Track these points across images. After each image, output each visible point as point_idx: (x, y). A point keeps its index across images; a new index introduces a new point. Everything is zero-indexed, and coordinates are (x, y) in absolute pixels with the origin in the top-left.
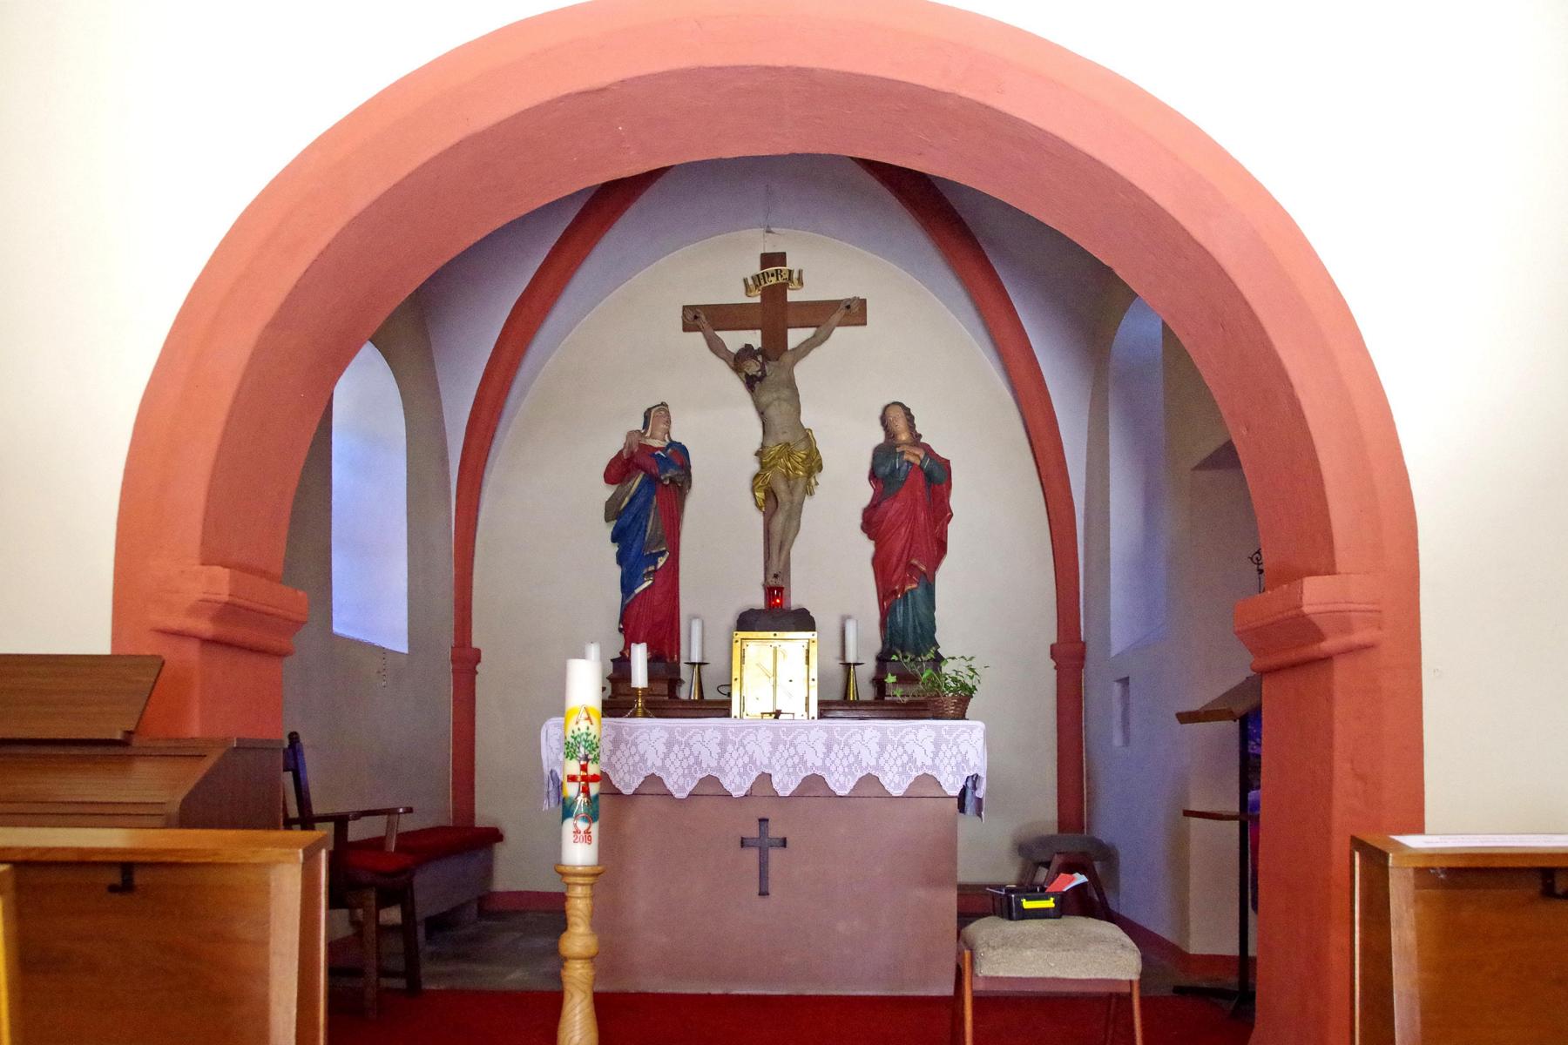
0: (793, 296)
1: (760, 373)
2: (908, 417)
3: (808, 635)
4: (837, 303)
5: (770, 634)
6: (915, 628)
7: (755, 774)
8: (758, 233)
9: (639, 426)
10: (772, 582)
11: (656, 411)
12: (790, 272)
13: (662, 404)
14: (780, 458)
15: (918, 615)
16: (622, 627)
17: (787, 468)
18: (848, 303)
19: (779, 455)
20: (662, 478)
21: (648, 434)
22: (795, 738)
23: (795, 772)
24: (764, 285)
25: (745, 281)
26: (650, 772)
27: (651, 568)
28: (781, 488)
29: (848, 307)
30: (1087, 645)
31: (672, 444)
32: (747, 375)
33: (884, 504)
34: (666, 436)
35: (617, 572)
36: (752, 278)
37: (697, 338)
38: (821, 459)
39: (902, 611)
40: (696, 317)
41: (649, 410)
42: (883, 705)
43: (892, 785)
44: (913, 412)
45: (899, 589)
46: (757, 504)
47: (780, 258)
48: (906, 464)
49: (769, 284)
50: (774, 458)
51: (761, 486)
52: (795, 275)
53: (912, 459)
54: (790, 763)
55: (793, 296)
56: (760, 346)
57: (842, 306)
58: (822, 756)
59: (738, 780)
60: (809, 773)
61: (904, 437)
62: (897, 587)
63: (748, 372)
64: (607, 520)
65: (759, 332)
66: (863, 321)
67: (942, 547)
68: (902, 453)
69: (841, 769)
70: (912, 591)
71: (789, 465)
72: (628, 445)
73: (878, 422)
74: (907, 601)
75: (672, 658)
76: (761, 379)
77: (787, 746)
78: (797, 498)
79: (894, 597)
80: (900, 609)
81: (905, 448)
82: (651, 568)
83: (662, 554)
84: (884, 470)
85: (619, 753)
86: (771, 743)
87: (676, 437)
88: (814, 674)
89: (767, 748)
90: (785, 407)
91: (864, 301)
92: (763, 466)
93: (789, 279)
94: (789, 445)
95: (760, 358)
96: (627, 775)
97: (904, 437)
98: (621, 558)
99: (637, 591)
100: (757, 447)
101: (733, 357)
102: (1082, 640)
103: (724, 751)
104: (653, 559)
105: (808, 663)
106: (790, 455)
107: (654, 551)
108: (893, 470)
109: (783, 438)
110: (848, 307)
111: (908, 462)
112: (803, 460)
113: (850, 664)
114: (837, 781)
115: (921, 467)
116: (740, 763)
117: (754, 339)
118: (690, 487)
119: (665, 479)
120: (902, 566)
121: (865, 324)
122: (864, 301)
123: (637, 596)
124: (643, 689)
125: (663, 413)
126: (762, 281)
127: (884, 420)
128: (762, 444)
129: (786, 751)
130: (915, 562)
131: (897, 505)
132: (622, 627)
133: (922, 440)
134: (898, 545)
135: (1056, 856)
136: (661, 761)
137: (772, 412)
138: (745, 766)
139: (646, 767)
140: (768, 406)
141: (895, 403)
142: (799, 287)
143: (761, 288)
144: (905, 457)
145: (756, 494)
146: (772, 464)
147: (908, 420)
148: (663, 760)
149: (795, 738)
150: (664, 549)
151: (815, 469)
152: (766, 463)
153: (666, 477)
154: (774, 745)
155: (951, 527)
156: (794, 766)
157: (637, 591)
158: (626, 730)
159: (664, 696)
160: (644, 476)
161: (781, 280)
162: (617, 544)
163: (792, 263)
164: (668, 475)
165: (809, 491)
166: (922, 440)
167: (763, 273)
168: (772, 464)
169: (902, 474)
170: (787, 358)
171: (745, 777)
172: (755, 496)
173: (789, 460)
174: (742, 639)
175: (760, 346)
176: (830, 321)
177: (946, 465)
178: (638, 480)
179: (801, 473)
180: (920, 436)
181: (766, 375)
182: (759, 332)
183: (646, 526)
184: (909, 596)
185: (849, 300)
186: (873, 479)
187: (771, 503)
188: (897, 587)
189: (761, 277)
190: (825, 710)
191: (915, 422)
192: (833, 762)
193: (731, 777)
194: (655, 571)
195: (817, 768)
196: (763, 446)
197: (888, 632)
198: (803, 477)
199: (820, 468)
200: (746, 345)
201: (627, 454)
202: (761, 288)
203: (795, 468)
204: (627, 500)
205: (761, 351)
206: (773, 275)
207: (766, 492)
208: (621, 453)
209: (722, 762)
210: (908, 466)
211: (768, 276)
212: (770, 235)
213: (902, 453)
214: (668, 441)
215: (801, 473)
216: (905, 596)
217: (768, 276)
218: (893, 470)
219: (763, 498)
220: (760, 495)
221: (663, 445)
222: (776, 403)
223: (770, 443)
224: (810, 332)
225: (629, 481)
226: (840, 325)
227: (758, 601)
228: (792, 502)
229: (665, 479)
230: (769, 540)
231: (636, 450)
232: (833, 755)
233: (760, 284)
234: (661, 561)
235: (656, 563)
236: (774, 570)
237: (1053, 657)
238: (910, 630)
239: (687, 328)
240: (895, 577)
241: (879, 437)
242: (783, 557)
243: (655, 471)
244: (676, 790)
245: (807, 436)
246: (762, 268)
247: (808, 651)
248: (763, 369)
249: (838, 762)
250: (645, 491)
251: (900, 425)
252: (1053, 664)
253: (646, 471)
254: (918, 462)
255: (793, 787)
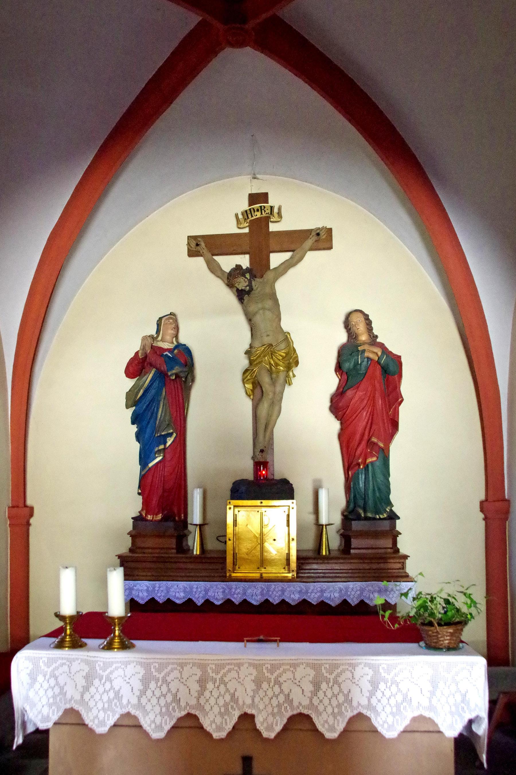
0: (273, 227)
1: (248, 288)
2: (367, 321)
3: (288, 502)
4: (310, 231)
5: (257, 502)
6: (374, 490)
7: (236, 714)
8: (245, 179)
9: (153, 332)
10: (260, 458)
11: (166, 319)
12: (272, 208)
13: (171, 314)
14: (265, 356)
15: (376, 481)
16: (140, 491)
17: (270, 363)
18: (318, 231)
19: (264, 354)
20: (169, 374)
21: (160, 338)
22: (280, 675)
23: (280, 712)
24: (251, 218)
25: (237, 215)
26: (125, 711)
27: (162, 447)
28: (266, 380)
29: (318, 234)
30: (512, 501)
31: (179, 346)
32: (238, 290)
33: (349, 393)
34: (174, 339)
35: (136, 446)
36: (242, 214)
37: (200, 261)
38: (297, 357)
39: (363, 477)
40: (197, 245)
41: (160, 319)
42: (349, 559)
43: (386, 726)
44: (370, 318)
45: (362, 462)
46: (246, 393)
47: (263, 197)
48: (366, 360)
49: (255, 217)
50: (259, 356)
51: (249, 379)
52: (276, 210)
53: (371, 356)
54: (275, 702)
55: (273, 227)
56: (248, 266)
57: (314, 233)
58: (310, 695)
59: (218, 720)
60: (295, 712)
61: (364, 338)
62: (360, 461)
63: (238, 287)
64: (127, 407)
65: (247, 257)
66: (330, 246)
67: (395, 425)
68: (364, 351)
69: (329, 710)
70: (372, 463)
71: (272, 362)
72: (143, 347)
73: (342, 326)
74: (368, 470)
75: (180, 517)
76: (249, 293)
77: (272, 684)
78: (278, 389)
79: (358, 467)
80: (362, 477)
81: (366, 347)
82: (162, 447)
83: (170, 435)
84: (347, 366)
85: (92, 690)
86: (253, 681)
87: (183, 340)
88: (294, 534)
89: (250, 686)
90: (268, 314)
91: (330, 230)
92: (251, 363)
93: (271, 213)
94: (272, 345)
95: (248, 276)
96: (101, 712)
97: (364, 338)
98: (139, 436)
99: (150, 465)
100: (247, 347)
101: (226, 275)
102: (506, 497)
103: (203, 688)
104: (163, 439)
105: (288, 525)
106: (272, 354)
107: (163, 433)
108: (356, 364)
109: (267, 340)
110: (318, 234)
111: (368, 358)
112: (284, 358)
113: (322, 525)
114: (326, 722)
115: (378, 362)
116: (221, 702)
117: (244, 261)
118: (193, 380)
119: (172, 375)
120: (364, 443)
121: (330, 248)
122: (330, 230)
123: (150, 469)
124: (120, 618)
125: (171, 321)
126: (250, 216)
127: (347, 324)
128: (250, 345)
129: (270, 690)
130: (374, 440)
131: (360, 394)
132: (140, 491)
133: (378, 340)
134: (361, 423)
135: (501, 696)
136: (137, 699)
137: (258, 319)
138: (226, 705)
139: (121, 704)
140: (255, 314)
141: (356, 311)
142: (279, 220)
143: (248, 221)
144: (366, 354)
145: (246, 385)
146: (257, 361)
147: (367, 324)
148: (139, 698)
149: (280, 675)
150: (171, 431)
151: (293, 364)
152: (254, 361)
153: (172, 373)
154: (258, 683)
155: (401, 408)
156: (279, 706)
157: (150, 465)
158: (99, 665)
159: (173, 549)
160: (156, 371)
161: (264, 215)
162: (136, 426)
163: (272, 201)
164: (174, 371)
165: (288, 381)
166: (378, 340)
167: (250, 209)
168: (257, 361)
169: (363, 368)
170: (269, 276)
171: (226, 717)
172: (245, 386)
173: (272, 358)
174: (234, 506)
175: (248, 266)
176: (304, 245)
177: (397, 360)
178: (151, 376)
179: (281, 368)
180: (377, 337)
181: (252, 289)
182: (247, 257)
183: (157, 414)
184: (370, 467)
185: (319, 228)
186: (339, 371)
187: (258, 391)
188: (360, 461)
189: (248, 212)
190: (302, 564)
191: (373, 325)
192: (321, 701)
193: (211, 716)
194: (164, 449)
195: (304, 707)
196: (251, 346)
197: (352, 496)
198: (283, 371)
199: (297, 363)
200: (236, 265)
201: (142, 355)
202: (248, 221)
203: (277, 365)
204: (141, 392)
205: (248, 270)
206: (258, 210)
207: (253, 383)
208: (137, 353)
209: (202, 701)
210: (368, 361)
211: (254, 211)
212: (255, 180)
213: (364, 351)
214: (175, 343)
215: (281, 368)
216: (366, 467)
217: (254, 211)
218: (356, 364)
219: (251, 388)
220: (249, 386)
221: (171, 346)
222: (261, 312)
223: (257, 344)
224: (287, 255)
225: (145, 375)
226: (311, 249)
227: (249, 474)
228: (274, 393)
229: (172, 375)
230: (256, 423)
231: (148, 352)
232: (321, 694)
233: (248, 218)
234: (170, 441)
235: (165, 443)
236: (260, 447)
237: (482, 510)
238: (370, 492)
239: (192, 253)
240: (358, 452)
241: (343, 338)
242: (268, 434)
243: (164, 368)
244: (152, 730)
245: (286, 338)
246: (250, 205)
247: (288, 516)
248: (250, 285)
249: (326, 701)
250: (156, 384)
251: (361, 328)
252: (482, 516)
253: (156, 368)
254: (376, 358)
255: (278, 728)
